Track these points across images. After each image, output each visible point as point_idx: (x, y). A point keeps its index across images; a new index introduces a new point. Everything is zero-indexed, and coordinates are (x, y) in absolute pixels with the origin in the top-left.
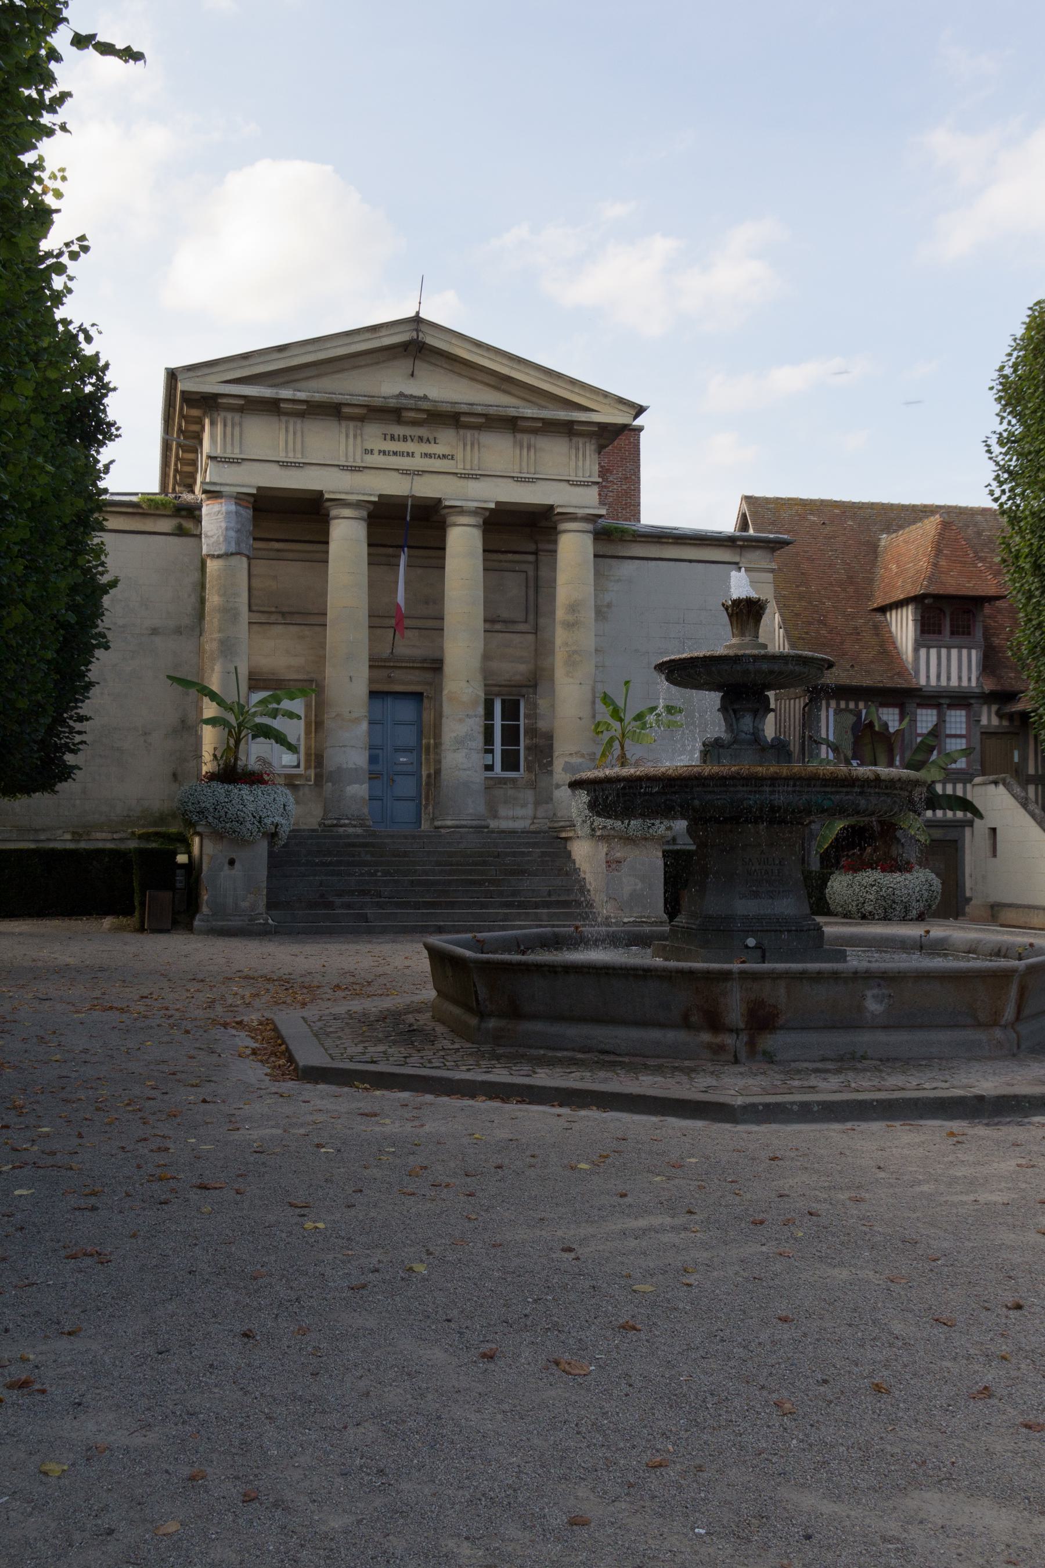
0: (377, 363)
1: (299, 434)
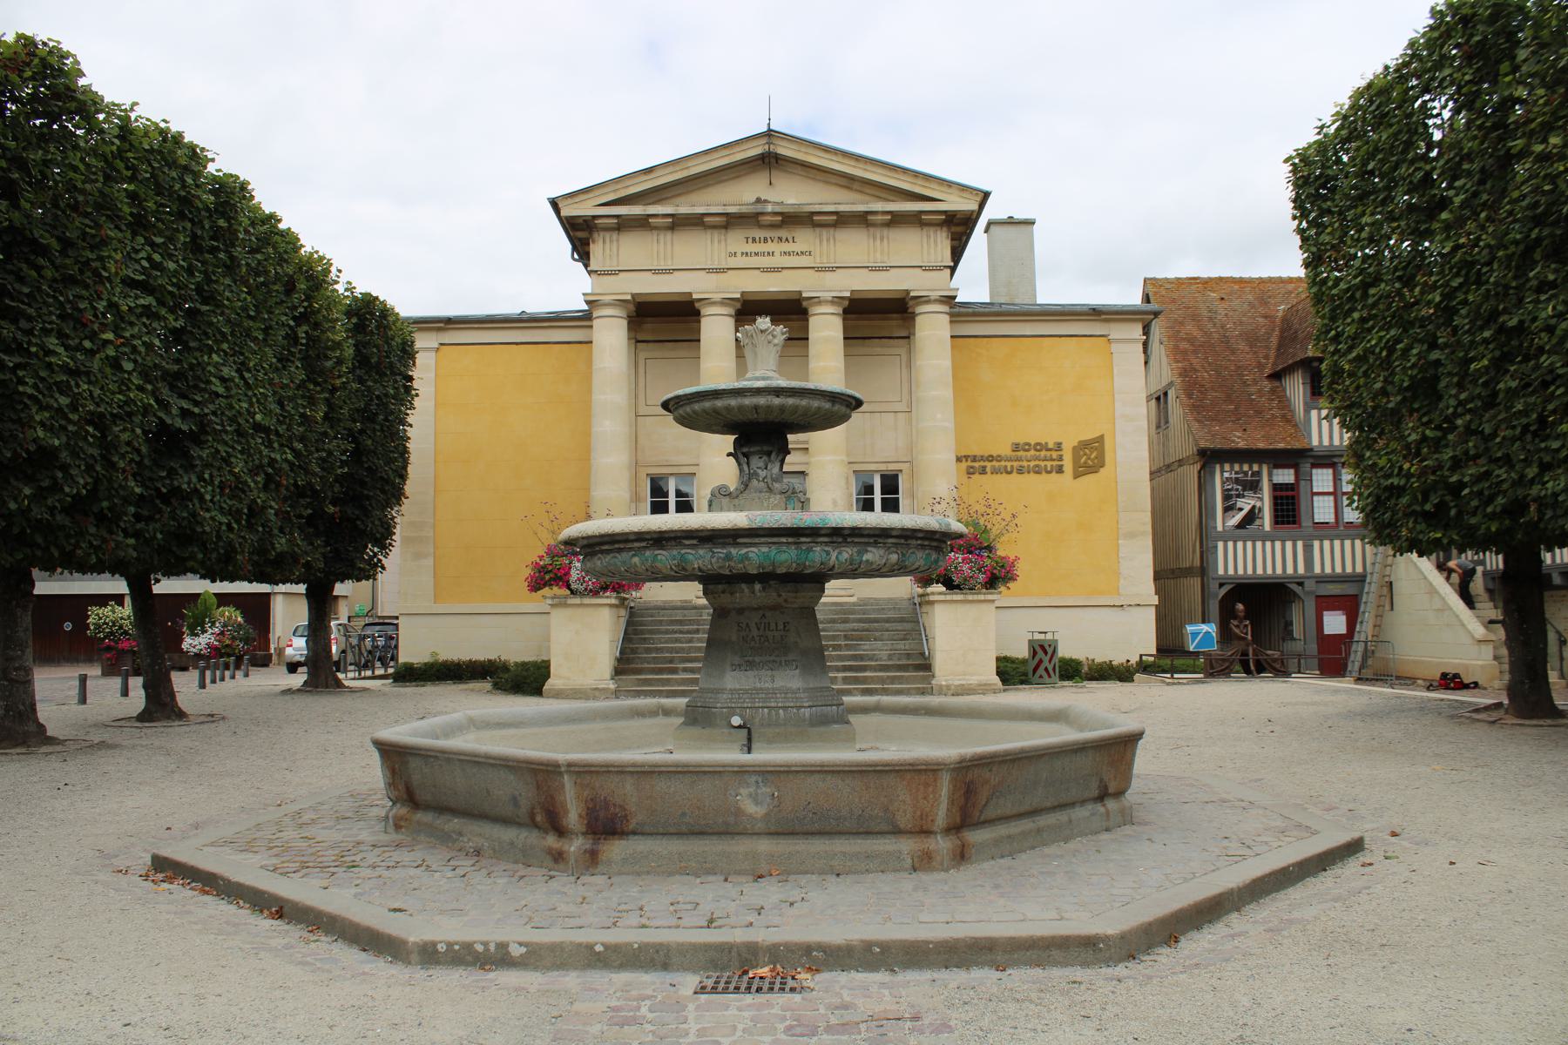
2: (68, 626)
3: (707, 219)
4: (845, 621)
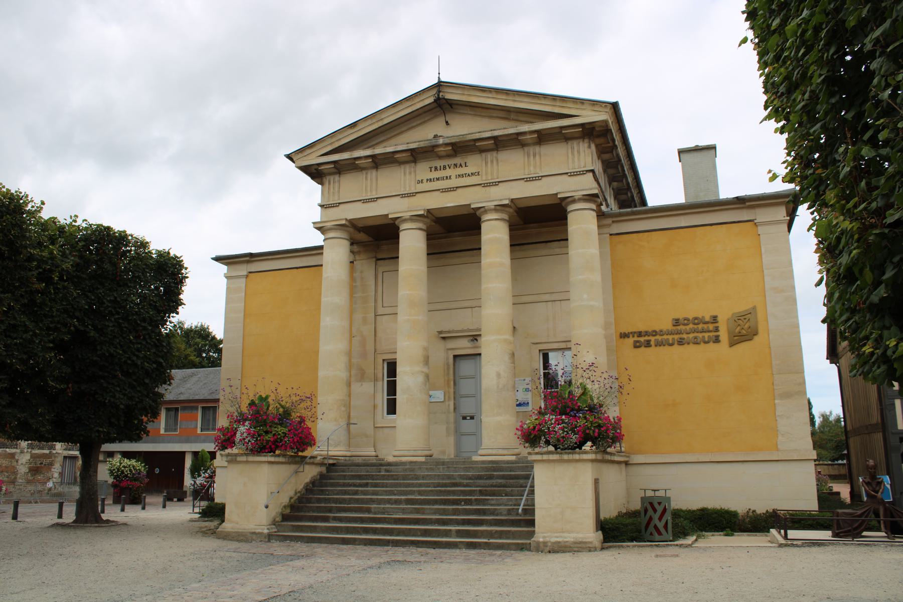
0: (424, 122)
1: (374, 180)
2: (157, 471)
3: (397, 156)
4: (491, 477)
